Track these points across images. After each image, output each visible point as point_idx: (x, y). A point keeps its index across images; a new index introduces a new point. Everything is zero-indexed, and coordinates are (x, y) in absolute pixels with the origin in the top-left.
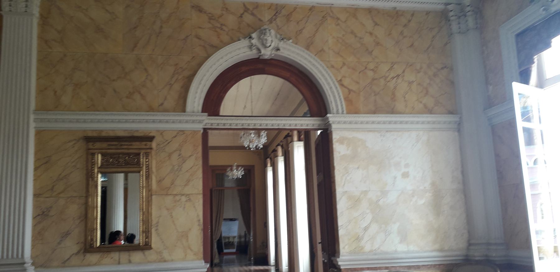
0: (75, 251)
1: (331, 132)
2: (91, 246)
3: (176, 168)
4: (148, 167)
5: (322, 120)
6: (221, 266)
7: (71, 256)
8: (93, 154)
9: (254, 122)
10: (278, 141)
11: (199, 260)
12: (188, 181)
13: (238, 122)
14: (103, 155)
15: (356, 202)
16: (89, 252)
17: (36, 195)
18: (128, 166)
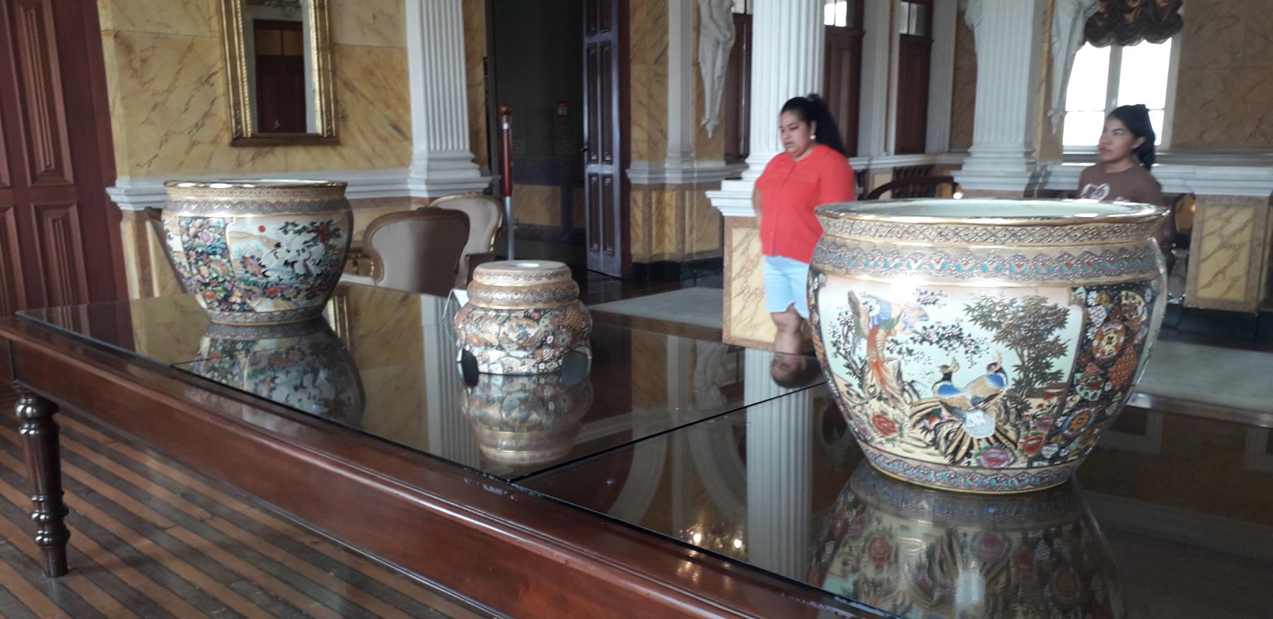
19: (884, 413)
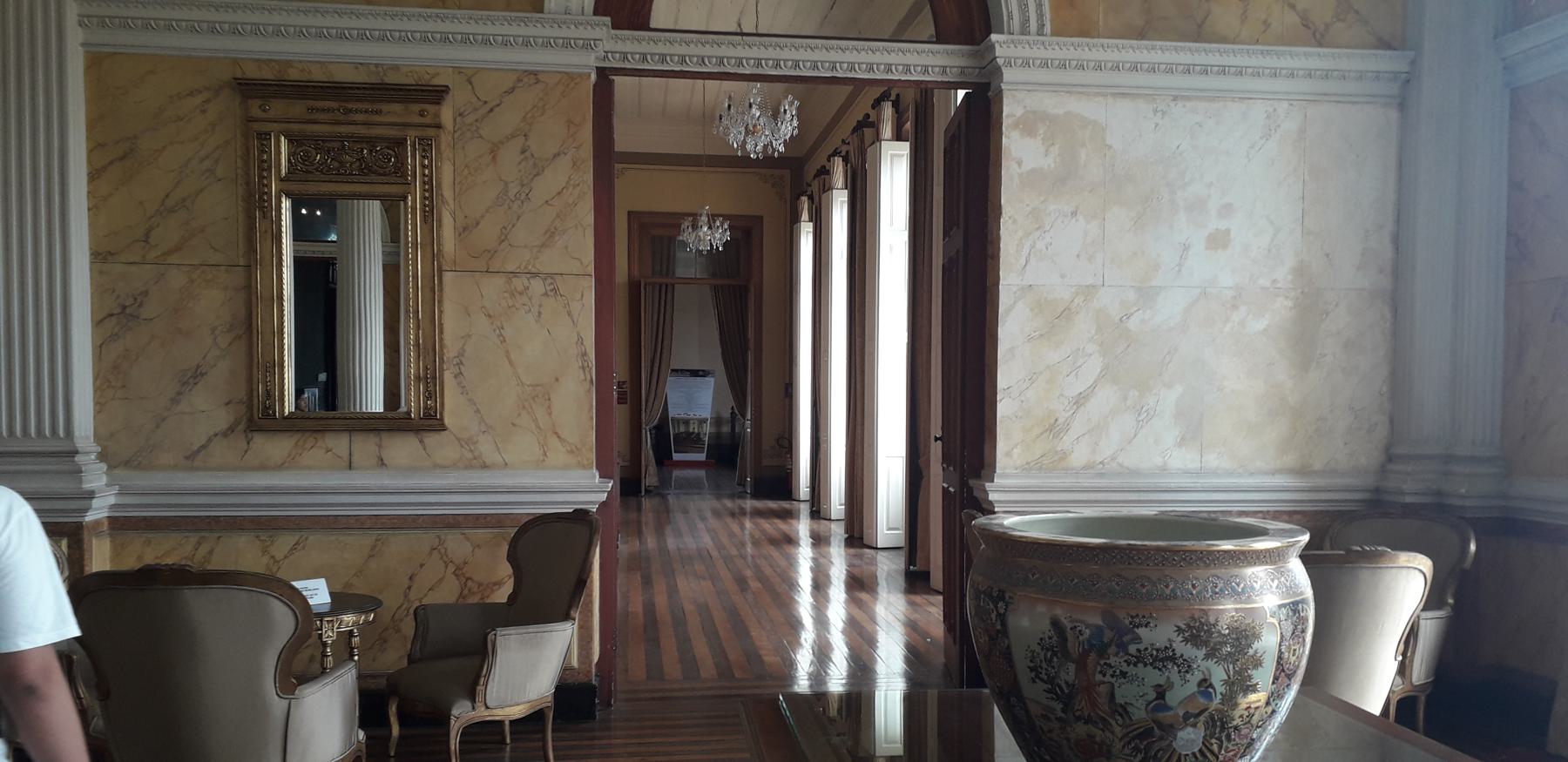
1: (999, 94)
2: (268, 413)
3: (513, 191)
4: (428, 183)
5: (973, 55)
7: (210, 440)
8: (264, 137)
9: (755, 53)
10: (834, 142)
11: (584, 467)
12: (551, 234)
13: (707, 51)
15: (1056, 318)
16: (260, 430)
17: (99, 256)
18: (368, 179)
19: (1091, 736)
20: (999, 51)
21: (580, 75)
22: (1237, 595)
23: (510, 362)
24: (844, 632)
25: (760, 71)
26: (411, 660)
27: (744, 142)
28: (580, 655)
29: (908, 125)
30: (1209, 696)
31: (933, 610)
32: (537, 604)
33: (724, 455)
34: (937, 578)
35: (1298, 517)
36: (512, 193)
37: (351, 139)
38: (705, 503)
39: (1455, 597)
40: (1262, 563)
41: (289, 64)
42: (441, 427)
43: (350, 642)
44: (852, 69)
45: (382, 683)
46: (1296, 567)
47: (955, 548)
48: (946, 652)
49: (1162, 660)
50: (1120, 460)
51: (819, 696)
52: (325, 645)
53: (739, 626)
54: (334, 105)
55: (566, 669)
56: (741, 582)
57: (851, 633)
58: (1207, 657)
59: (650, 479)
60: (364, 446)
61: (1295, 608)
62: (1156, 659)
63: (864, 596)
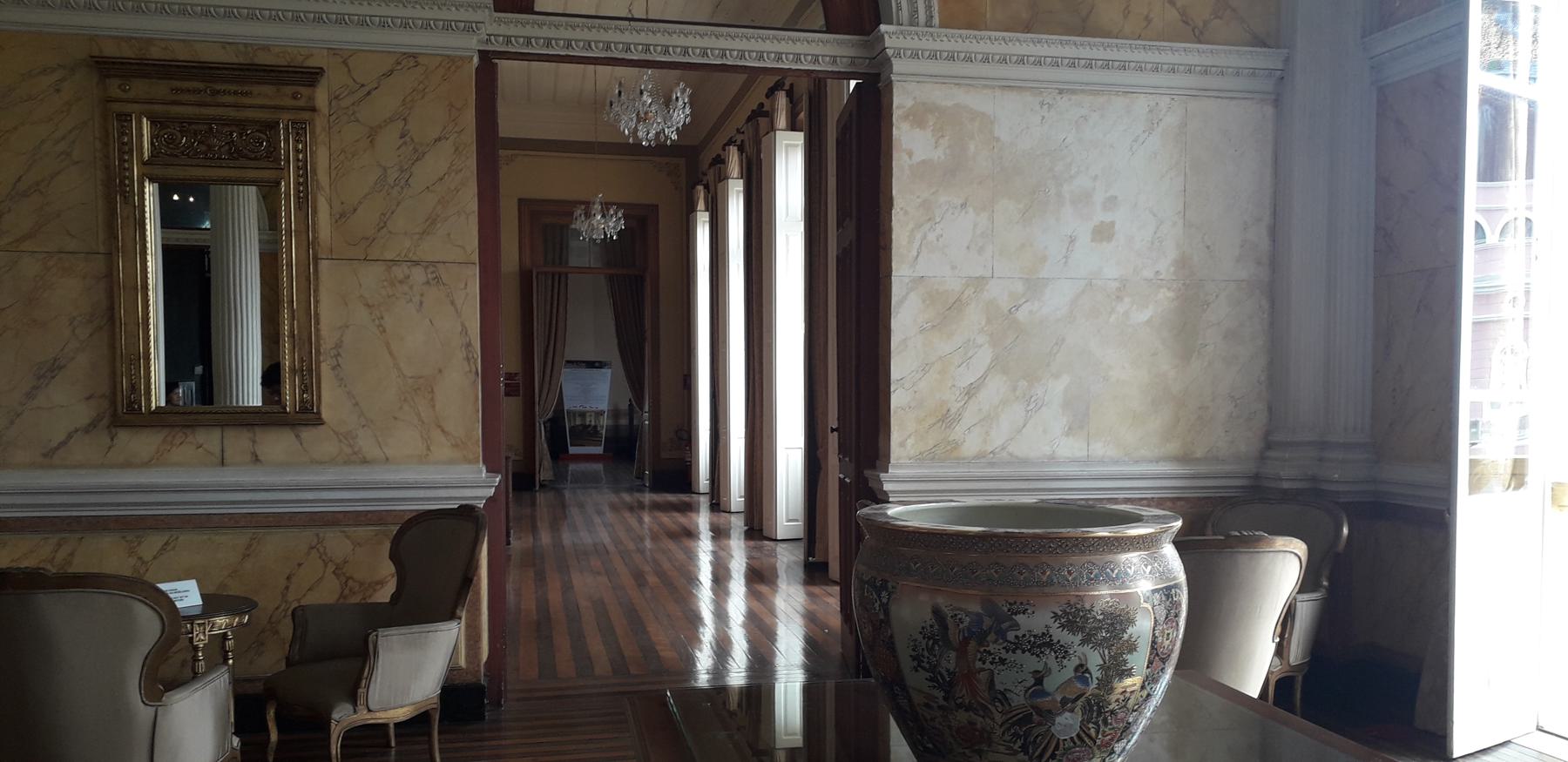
0: (84, 421)
1: (889, 85)
2: (133, 407)
4: (302, 168)
6: (559, 493)
7: (70, 436)
8: (124, 118)
9: (643, 38)
10: (729, 131)
11: (470, 462)
12: (432, 220)
14: (153, 122)
19: (972, 724)
20: (888, 42)
21: (461, 58)
22: (1111, 581)
23: (391, 353)
24: (746, 626)
25: (648, 57)
26: (289, 662)
27: (636, 130)
28: (467, 656)
29: (802, 115)
30: (1086, 682)
31: (831, 600)
32: (421, 604)
33: (622, 448)
34: (834, 569)
35: (1172, 504)
36: (391, 181)
37: (225, 121)
38: (603, 497)
39: (1330, 580)
40: (1136, 549)
41: (150, 41)
42: (318, 421)
43: (224, 646)
44: (742, 57)
45: (259, 687)
46: (1169, 552)
47: (851, 541)
48: (843, 645)
49: (1040, 646)
50: (1010, 449)
51: (719, 690)
52: (196, 649)
53: (635, 621)
54: (201, 86)
55: (452, 670)
56: (639, 577)
57: (749, 627)
58: (1083, 642)
59: (545, 472)
60: (238, 441)
61: (1168, 592)
62: (1033, 645)
63: (763, 588)
